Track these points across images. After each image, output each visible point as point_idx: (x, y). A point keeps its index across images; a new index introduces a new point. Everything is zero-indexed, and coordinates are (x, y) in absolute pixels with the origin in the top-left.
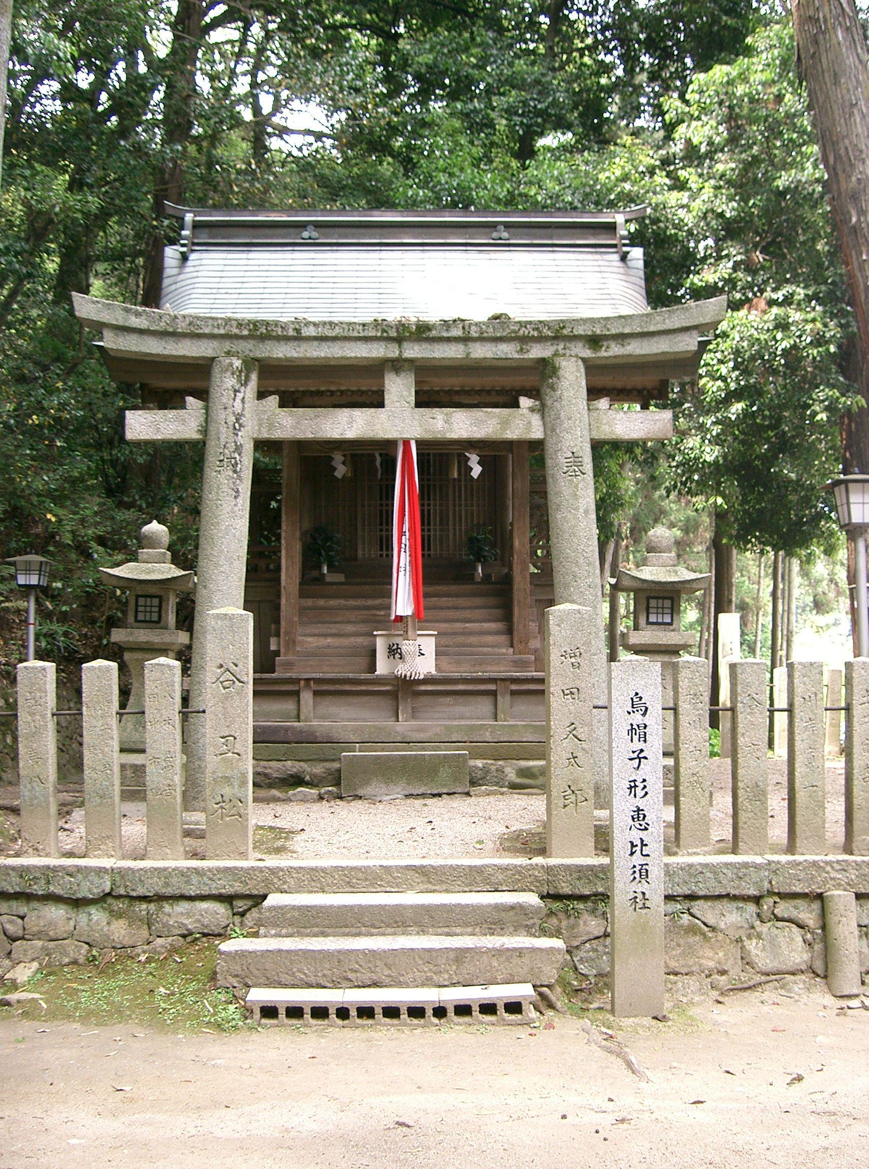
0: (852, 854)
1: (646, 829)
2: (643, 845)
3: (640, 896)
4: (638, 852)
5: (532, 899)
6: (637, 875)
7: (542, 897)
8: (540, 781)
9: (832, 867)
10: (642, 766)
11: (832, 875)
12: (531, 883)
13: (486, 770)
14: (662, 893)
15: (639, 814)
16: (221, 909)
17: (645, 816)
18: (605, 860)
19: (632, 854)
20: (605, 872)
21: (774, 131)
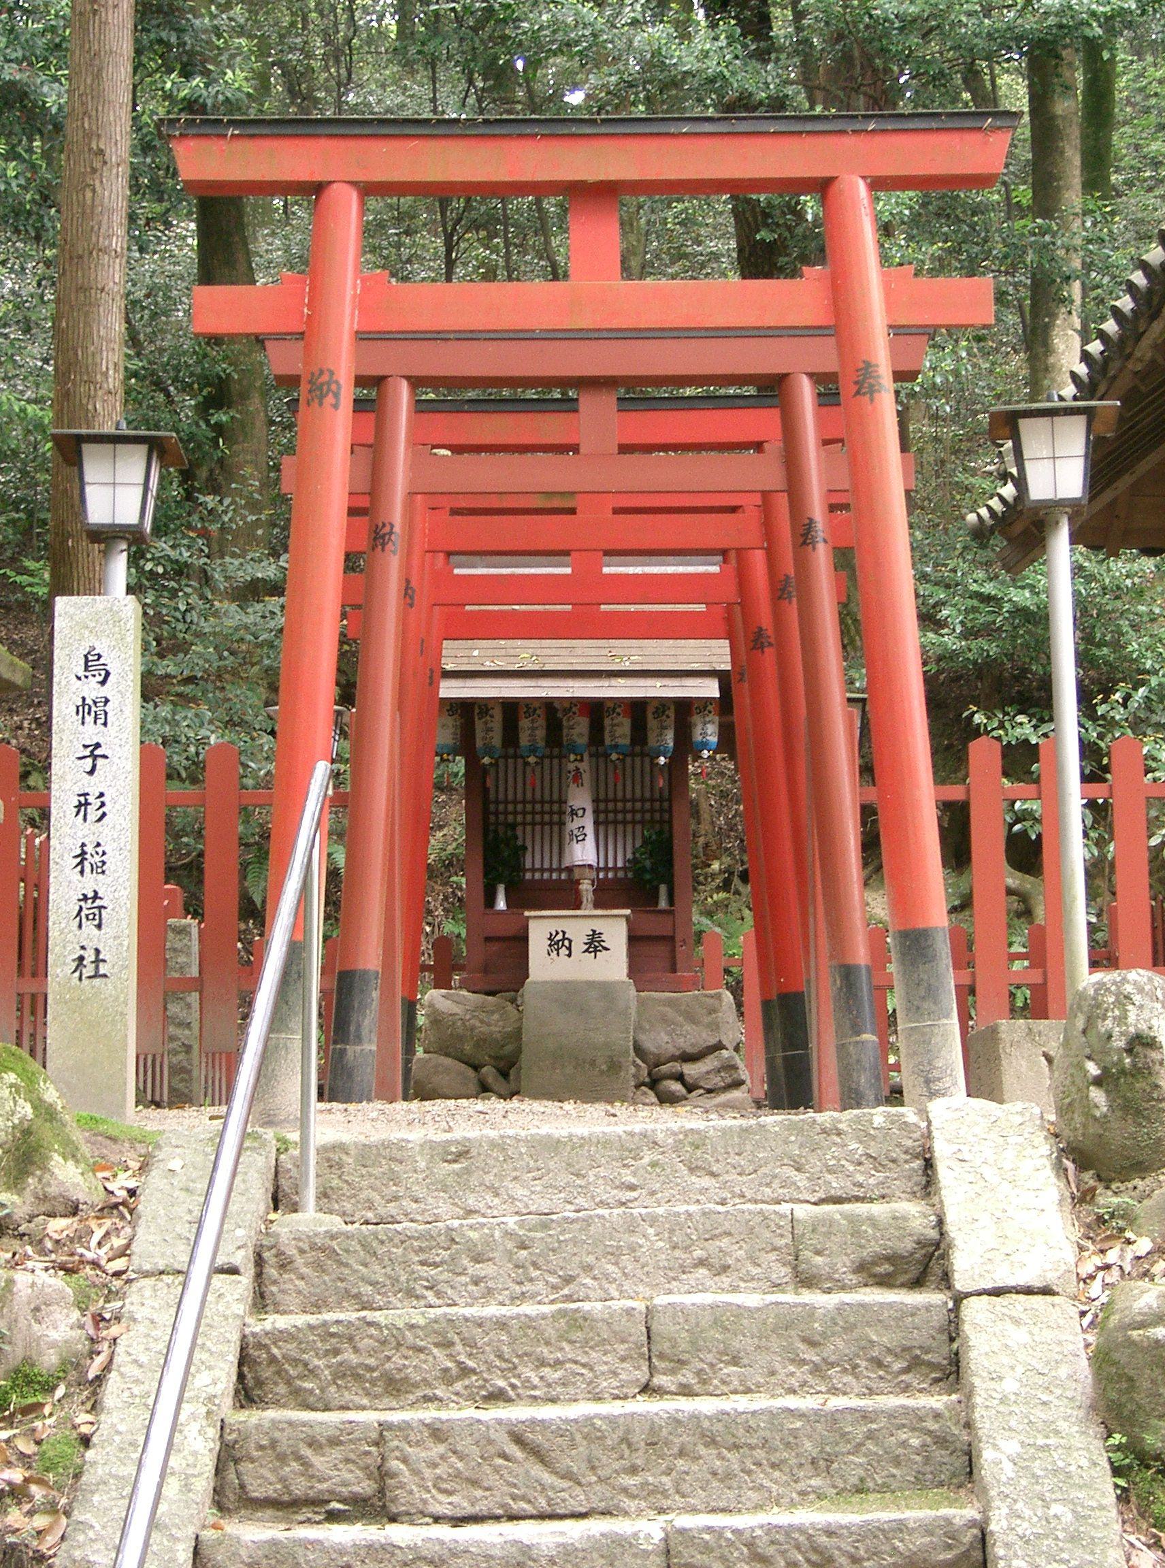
3: (90, 956)
15: (94, 753)
21: (29, 432)
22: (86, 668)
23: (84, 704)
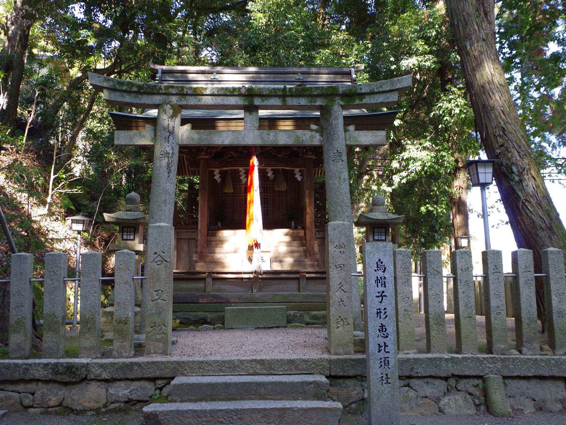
0: (492, 353)
1: (387, 337)
2: (386, 346)
3: (385, 376)
4: (383, 350)
5: (323, 379)
6: (383, 364)
7: (327, 377)
8: (322, 321)
9: (488, 361)
10: (384, 300)
11: (488, 365)
12: (321, 369)
13: (295, 316)
14: (397, 374)
15: (382, 328)
16: (150, 386)
17: (386, 329)
18: (364, 356)
19: (379, 351)
20: (363, 362)
22: (378, 267)
23: (378, 279)
